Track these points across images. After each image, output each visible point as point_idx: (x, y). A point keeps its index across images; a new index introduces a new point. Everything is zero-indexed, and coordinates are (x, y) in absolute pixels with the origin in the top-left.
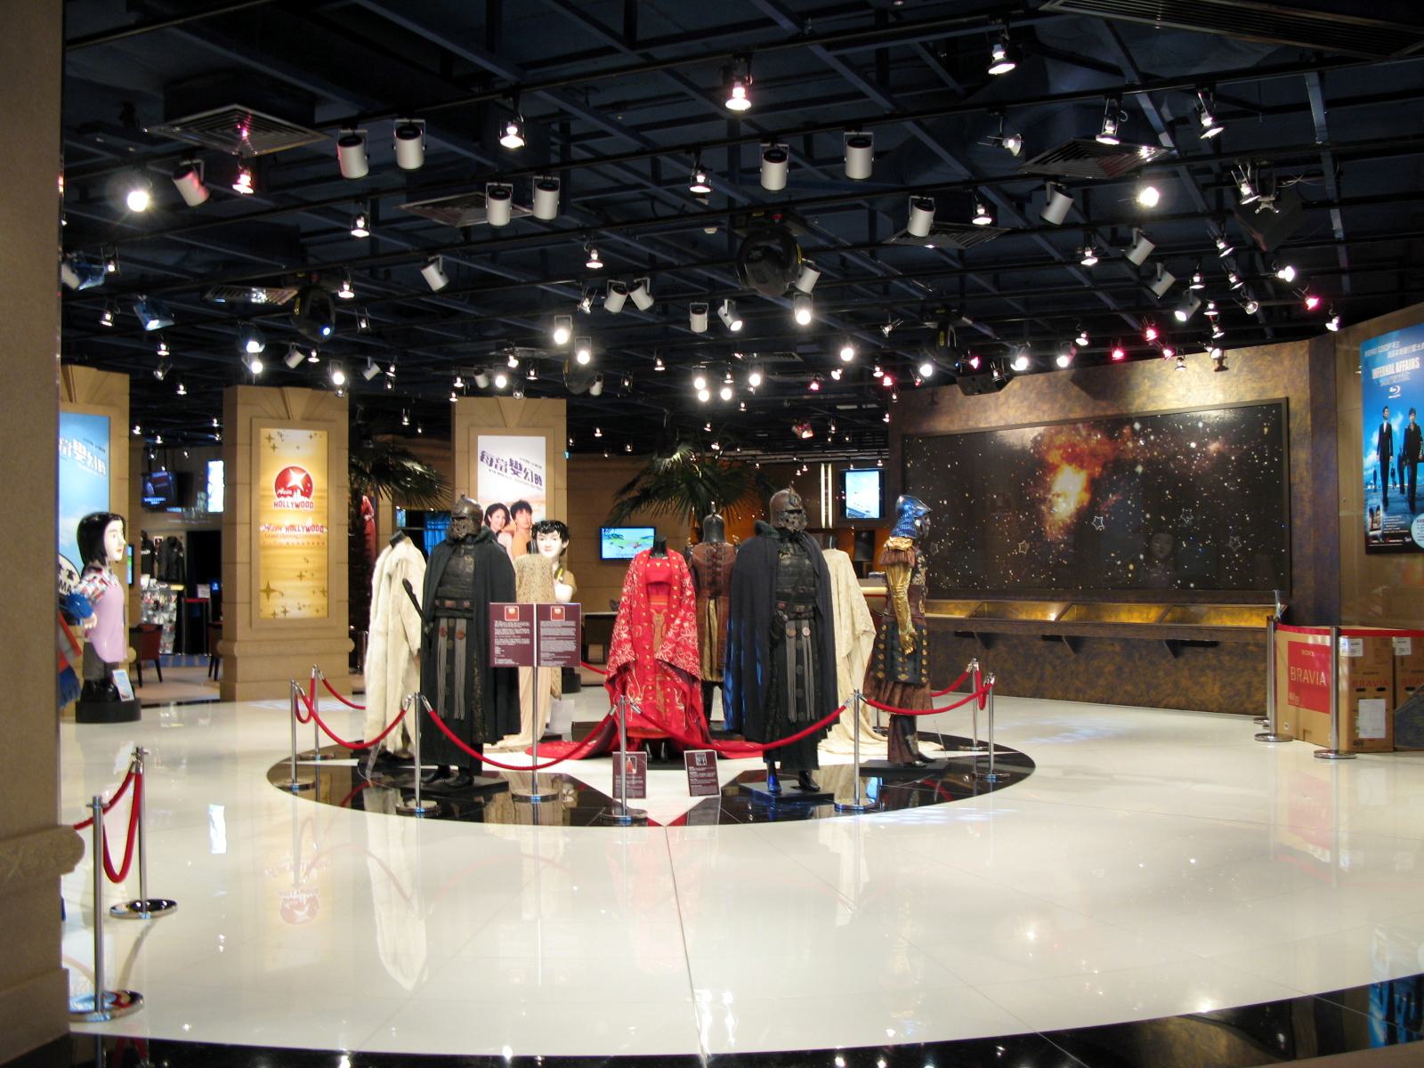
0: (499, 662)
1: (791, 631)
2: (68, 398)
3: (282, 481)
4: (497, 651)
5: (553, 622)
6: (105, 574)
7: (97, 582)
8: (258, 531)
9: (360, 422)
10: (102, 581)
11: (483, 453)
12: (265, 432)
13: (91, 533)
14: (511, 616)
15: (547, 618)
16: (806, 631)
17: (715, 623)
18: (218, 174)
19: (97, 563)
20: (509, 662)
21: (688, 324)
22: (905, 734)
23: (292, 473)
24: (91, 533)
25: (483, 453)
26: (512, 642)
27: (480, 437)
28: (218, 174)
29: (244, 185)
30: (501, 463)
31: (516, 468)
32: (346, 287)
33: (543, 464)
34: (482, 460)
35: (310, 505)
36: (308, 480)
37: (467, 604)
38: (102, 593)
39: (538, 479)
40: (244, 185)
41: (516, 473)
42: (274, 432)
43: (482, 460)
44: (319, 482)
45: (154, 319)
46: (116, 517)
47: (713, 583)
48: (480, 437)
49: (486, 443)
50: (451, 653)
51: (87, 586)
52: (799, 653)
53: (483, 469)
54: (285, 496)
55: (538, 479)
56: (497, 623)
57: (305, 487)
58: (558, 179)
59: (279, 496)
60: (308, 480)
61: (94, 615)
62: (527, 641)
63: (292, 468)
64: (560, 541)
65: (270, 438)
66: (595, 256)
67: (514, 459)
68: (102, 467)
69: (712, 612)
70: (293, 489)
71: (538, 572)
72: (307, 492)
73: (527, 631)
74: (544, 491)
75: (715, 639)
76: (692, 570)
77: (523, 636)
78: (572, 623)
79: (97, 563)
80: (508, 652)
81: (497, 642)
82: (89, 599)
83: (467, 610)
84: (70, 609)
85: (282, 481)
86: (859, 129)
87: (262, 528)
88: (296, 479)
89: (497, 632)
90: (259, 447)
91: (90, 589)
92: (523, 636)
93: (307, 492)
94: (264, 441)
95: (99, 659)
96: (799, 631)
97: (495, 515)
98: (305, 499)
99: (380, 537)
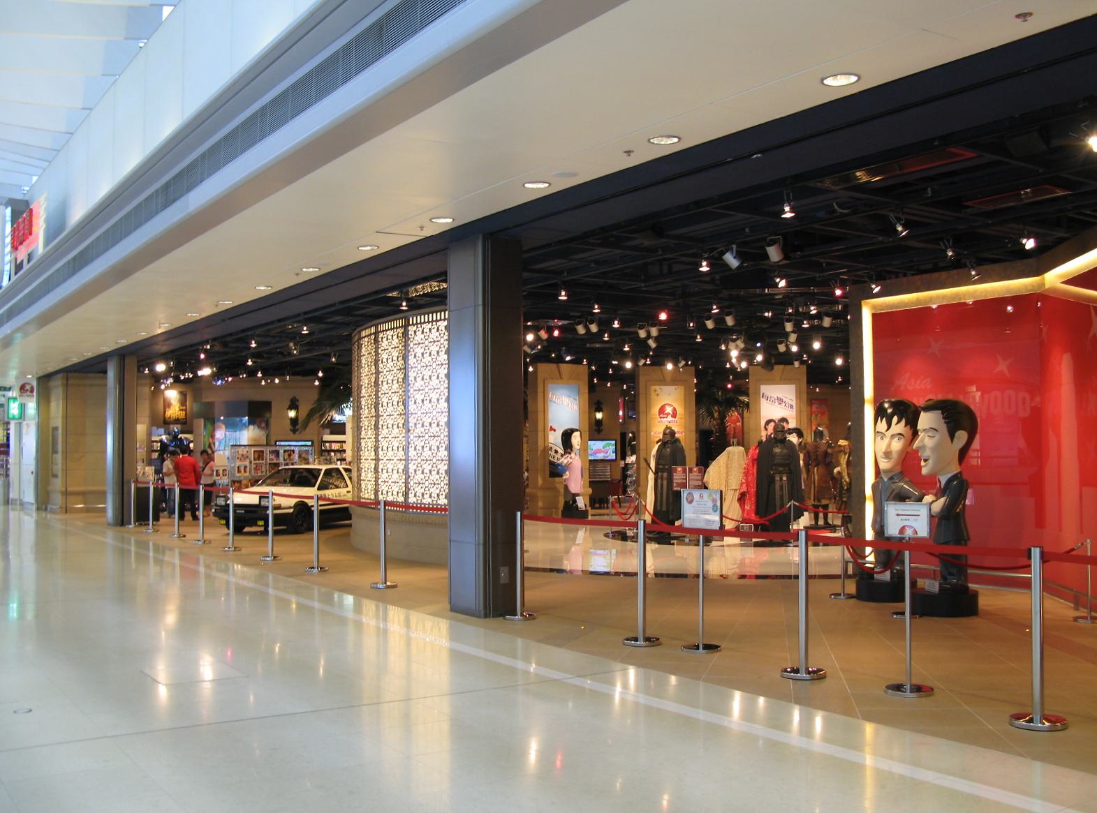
0: (675, 489)
1: (777, 478)
2: (559, 377)
3: (662, 410)
4: (675, 484)
5: (694, 474)
6: (573, 455)
7: (568, 458)
8: (650, 434)
9: (710, 378)
10: (571, 458)
11: (763, 394)
12: (653, 388)
13: (567, 436)
14: (679, 472)
15: (692, 472)
16: (785, 478)
17: (816, 478)
18: (550, 330)
19: (569, 450)
20: (679, 489)
21: (777, 349)
22: (847, 523)
23: (667, 407)
24: (567, 436)
25: (763, 394)
26: (679, 481)
27: (762, 386)
28: (550, 330)
29: (556, 333)
30: (772, 399)
31: (780, 401)
32: (626, 346)
33: (794, 399)
34: (763, 397)
35: (676, 422)
36: (674, 410)
37: (667, 467)
38: (571, 463)
39: (791, 406)
40: (556, 333)
41: (780, 404)
42: (657, 388)
43: (763, 397)
44: (680, 410)
45: (568, 356)
46: (577, 430)
47: (816, 459)
48: (762, 386)
49: (765, 389)
50: (662, 485)
51: (564, 461)
52: (781, 487)
53: (763, 402)
54: (664, 418)
55: (791, 406)
56: (675, 474)
57: (673, 413)
58: (930, 195)
59: (661, 418)
60: (674, 410)
61: (567, 473)
62: (685, 481)
63: (667, 404)
64: (797, 438)
65: (655, 391)
66: (699, 337)
67: (779, 397)
68: (576, 407)
69: (815, 473)
70: (668, 414)
71: (737, 454)
72: (674, 415)
73: (685, 477)
74: (795, 413)
75: (816, 485)
76: (807, 455)
77: (684, 479)
78: (700, 474)
79: (569, 450)
80: (679, 485)
81: (675, 481)
82: (565, 466)
83: (667, 469)
84: (556, 471)
85: (662, 410)
86: (729, 309)
87: (652, 433)
88: (669, 410)
89: (675, 477)
90: (650, 394)
91: (565, 461)
92: (684, 479)
93: (674, 415)
94: (652, 392)
95: (570, 492)
96: (781, 479)
97: (770, 425)
98: (673, 419)
99: (745, 435)
